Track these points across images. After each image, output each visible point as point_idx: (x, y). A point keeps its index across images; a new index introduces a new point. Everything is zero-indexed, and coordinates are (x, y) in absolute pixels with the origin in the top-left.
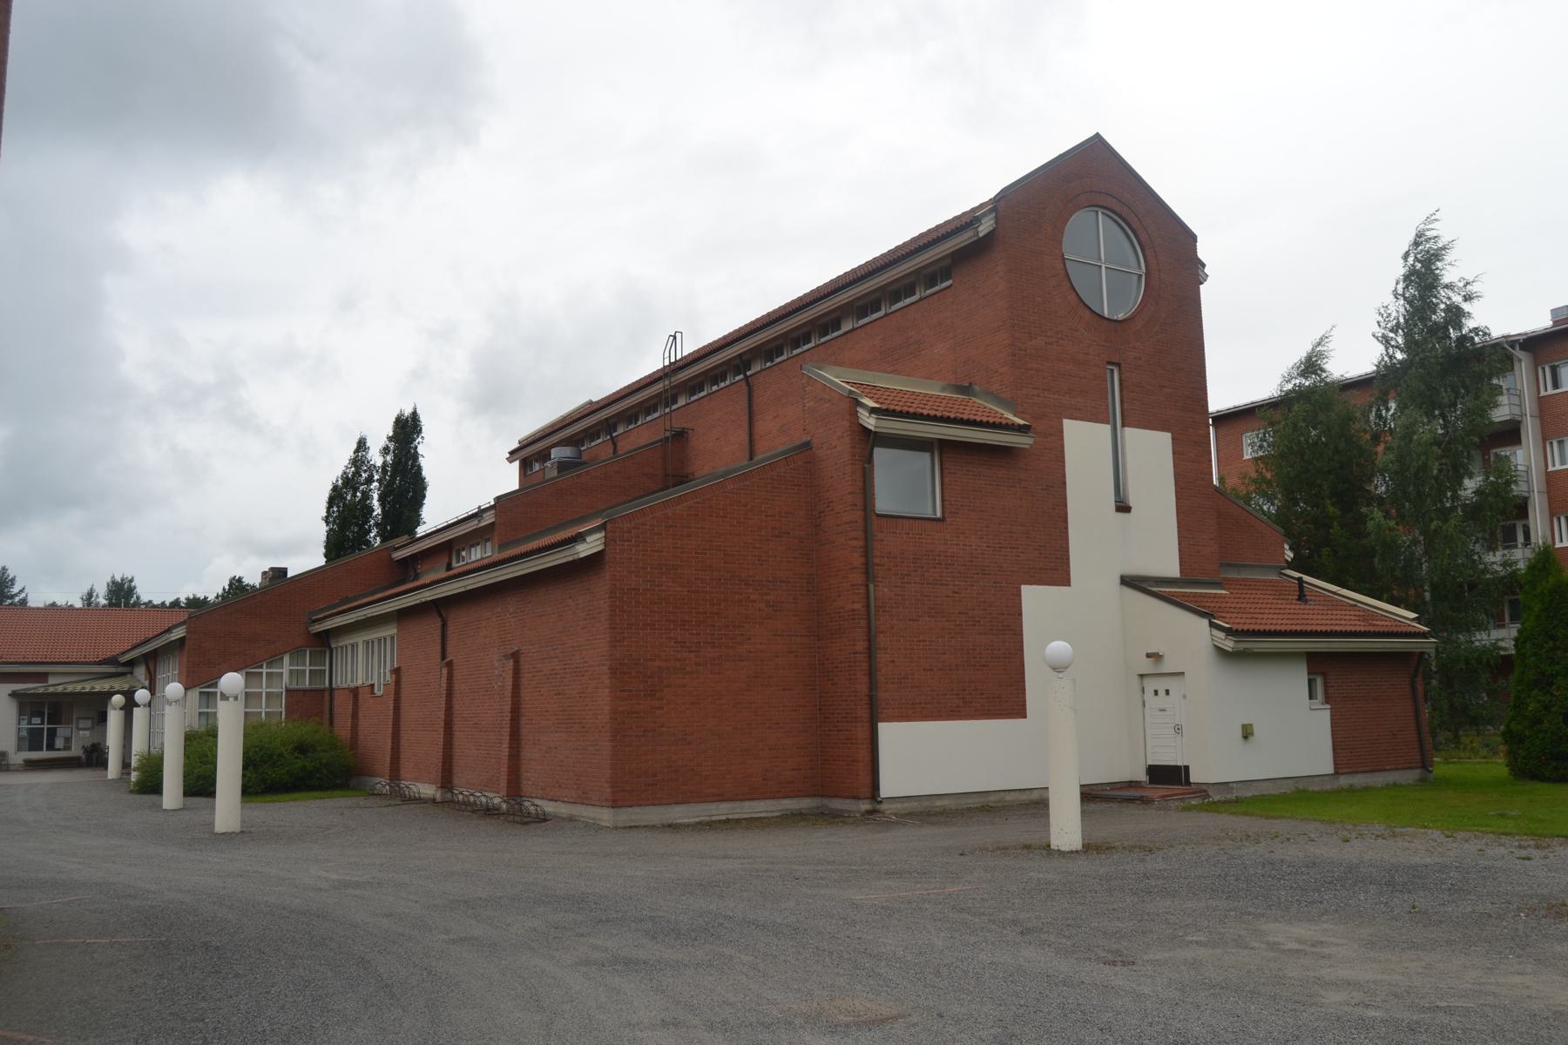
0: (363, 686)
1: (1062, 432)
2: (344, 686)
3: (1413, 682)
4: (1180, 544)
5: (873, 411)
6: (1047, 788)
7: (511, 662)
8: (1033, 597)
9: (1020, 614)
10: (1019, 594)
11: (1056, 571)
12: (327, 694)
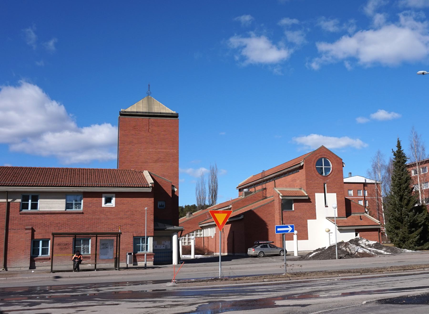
0: (209, 236)
1: (315, 195)
2: (206, 236)
3: (199, 250)
4: (338, 211)
5: (281, 196)
6: (294, 251)
7: (232, 233)
8: (309, 221)
9: (307, 224)
10: (307, 221)
11: (314, 217)
12: (203, 238)
